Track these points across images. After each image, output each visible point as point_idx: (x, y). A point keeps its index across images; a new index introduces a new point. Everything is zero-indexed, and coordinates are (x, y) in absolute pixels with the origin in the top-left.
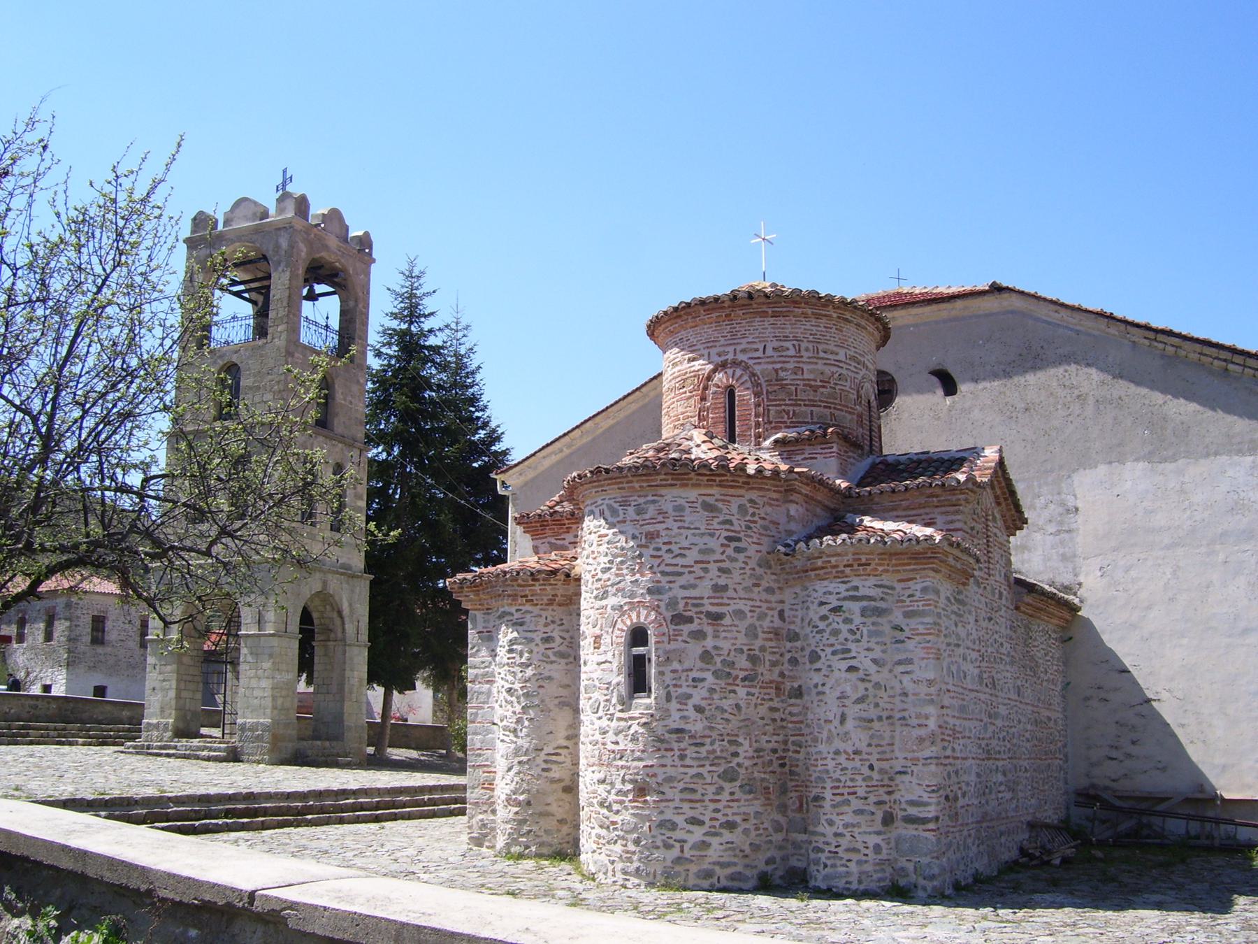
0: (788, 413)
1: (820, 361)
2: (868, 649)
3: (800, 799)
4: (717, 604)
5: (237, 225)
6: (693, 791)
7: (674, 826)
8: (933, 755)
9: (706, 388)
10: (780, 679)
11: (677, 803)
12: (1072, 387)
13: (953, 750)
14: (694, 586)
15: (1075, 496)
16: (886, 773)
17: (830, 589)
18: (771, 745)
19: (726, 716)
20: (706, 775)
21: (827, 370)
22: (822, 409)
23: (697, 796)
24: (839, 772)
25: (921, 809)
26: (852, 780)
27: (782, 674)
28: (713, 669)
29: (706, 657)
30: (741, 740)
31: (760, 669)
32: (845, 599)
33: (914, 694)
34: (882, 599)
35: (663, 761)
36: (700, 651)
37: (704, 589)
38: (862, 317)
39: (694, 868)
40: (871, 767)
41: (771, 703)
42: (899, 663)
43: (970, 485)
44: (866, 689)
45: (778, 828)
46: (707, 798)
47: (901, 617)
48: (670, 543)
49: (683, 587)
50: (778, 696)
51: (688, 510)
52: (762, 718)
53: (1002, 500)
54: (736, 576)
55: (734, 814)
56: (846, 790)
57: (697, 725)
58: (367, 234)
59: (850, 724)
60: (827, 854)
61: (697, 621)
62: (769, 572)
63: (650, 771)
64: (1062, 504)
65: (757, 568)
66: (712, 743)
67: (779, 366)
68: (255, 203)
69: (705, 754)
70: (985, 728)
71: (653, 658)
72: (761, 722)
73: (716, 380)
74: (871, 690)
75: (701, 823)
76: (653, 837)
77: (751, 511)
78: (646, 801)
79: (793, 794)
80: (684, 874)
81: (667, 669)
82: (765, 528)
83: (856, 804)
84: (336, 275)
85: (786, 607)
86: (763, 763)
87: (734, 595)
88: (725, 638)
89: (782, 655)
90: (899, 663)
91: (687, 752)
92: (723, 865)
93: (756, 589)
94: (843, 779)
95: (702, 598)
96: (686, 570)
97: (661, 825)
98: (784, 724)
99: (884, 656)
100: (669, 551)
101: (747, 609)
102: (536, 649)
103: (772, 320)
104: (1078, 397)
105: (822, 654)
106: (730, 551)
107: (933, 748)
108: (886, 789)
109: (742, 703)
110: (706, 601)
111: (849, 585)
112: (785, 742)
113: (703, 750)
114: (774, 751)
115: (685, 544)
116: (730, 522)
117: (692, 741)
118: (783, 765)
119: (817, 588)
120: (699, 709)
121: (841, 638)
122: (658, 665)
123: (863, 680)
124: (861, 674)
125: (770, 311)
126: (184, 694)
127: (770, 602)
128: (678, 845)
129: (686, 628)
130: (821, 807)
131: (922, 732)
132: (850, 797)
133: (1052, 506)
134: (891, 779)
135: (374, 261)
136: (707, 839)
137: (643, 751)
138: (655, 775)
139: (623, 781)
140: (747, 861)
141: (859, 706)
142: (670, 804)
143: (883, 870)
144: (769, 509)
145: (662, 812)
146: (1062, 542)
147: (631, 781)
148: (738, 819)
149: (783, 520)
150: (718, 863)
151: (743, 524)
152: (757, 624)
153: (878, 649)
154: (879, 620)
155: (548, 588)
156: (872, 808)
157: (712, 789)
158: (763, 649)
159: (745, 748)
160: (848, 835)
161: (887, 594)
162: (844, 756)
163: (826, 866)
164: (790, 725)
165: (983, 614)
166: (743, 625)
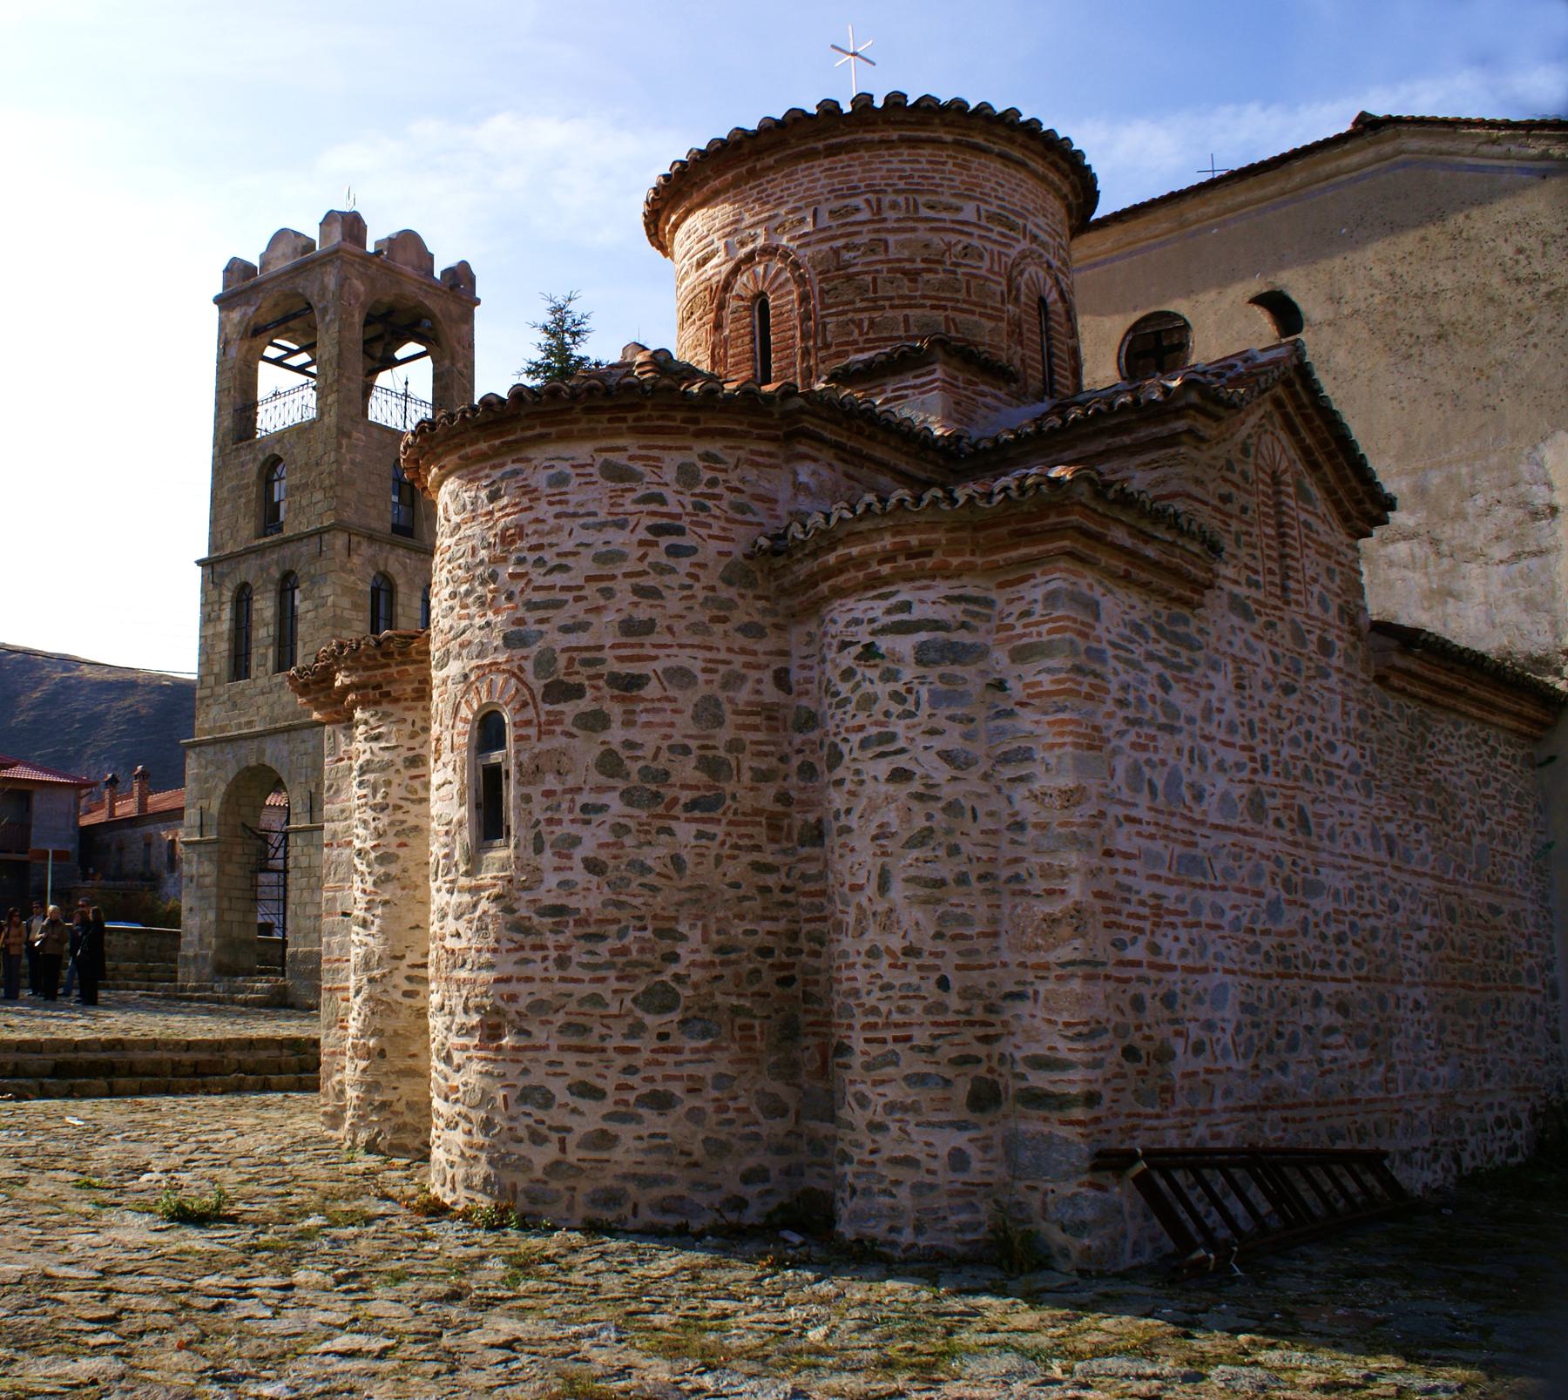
0: (859, 324)
1: (920, 225)
2: (933, 732)
3: (823, 1049)
4: (631, 659)
5: (272, 269)
6: (583, 1030)
7: (547, 1100)
8: (1077, 956)
9: (721, 306)
10: (779, 808)
11: (553, 1054)
12: (1534, 279)
13: (1154, 949)
14: (583, 627)
15: (1549, 485)
16: (979, 996)
17: (857, 614)
18: (756, 941)
19: (650, 879)
20: (608, 997)
21: (937, 240)
22: (927, 312)
23: (593, 1041)
24: (877, 994)
25: (1056, 1076)
26: (901, 1010)
27: (784, 798)
28: (622, 785)
29: (610, 763)
30: (683, 928)
31: (728, 787)
32: (885, 630)
33: (1036, 825)
34: (964, 625)
35: (528, 970)
36: (597, 751)
37: (605, 629)
38: (1011, 141)
39: (585, 1187)
40: (943, 984)
41: (756, 856)
42: (1005, 759)
43: (1193, 397)
44: (929, 817)
45: (775, 1109)
46: (610, 1044)
47: (1005, 660)
48: (540, 547)
49: (566, 629)
50: (773, 840)
51: (575, 481)
52: (735, 885)
53: (1320, 457)
54: (673, 604)
55: (667, 1078)
56: (888, 1034)
57: (591, 899)
58: (464, 266)
59: (898, 892)
60: (855, 1167)
61: (589, 693)
62: (750, 593)
63: (505, 989)
64: (1523, 504)
65: (720, 585)
66: (622, 934)
67: (840, 243)
68: (298, 235)
69: (605, 956)
70: (1274, 910)
71: (513, 770)
72: (730, 893)
73: (737, 288)
74: (939, 816)
75: (596, 1094)
76: (512, 1119)
77: (706, 475)
78: (499, 1049)
79: (811, 1041)
80: (567, 1195)
81: (535, 792)
82: (741, 508)
83: (912, 1063)
84: (417, 323)
85: (794, 664)
86: (737, 976)
87: (668, 639)
88: (648, 724)
89: (783, 759)
90: (1005, 759)
91: (572, 952)
92: (646, 1181)
93: (718, 628)
94: (884, 1007)
95: (600, 648)
96: (569, 596)
97: (526, 1096)
98: (790, 897)
99: (969, 746)
100: (540, 562)
101: (697, 667)
102: (396, 780)
103: (826, 163)
104: (1548, 295)
105: (845, 748)
106: (658, 555)
107: (1077, 943)
108: (980, 1031)
109: (686, 855)
110: (607, 654)
111: (893, 601)
112: (793, 936)
113: (603, 949)
114: (765, 952)
115: (568, 545)
116: (659, 499)
117: (580, 931)
118: (786, 982)
119: (835, 615)
120: (593, 866)
121: (878, 710)
122: (519, 783)
123: (919, 797)
124: (916, 786)
125: (820, 145)
126: (228, 916)
127: (755, 653)
128: (554, 1136)
129: (570, 709)
130: (847, 1067)
131: (1056, 907)
132: (898, 1048)
133: (1501, 511)
134: (991, 1009)
135: (478, 302)
136: (613, 1127)
137: (495, 951)
138: (513, 998)
139: (466, 1010)
140: (696, 1174)
141: (915, 853)
142: (540, 1055)
143: (972, 1207)
144: (752, 474)
145: (525, 1071)
146: (1526, 577)
147: (478, 1009)
148: (677, 1089)
149: (784, 493)
150: (634, 1177)
151: (688, 500)
152: (722, 696)
153: (956, 730)
154: (957, 670)
155: (411, 668)
156: (949, 1073)
157: (619, 1028)
158: (735, 746)
159: (693, 948)
160: (894, 1128)
161: (975, 615)
162: (886, 960)
163: (854, 1192)
164: (803, 900)
165: (1262, 674)
166: (688, 699)
